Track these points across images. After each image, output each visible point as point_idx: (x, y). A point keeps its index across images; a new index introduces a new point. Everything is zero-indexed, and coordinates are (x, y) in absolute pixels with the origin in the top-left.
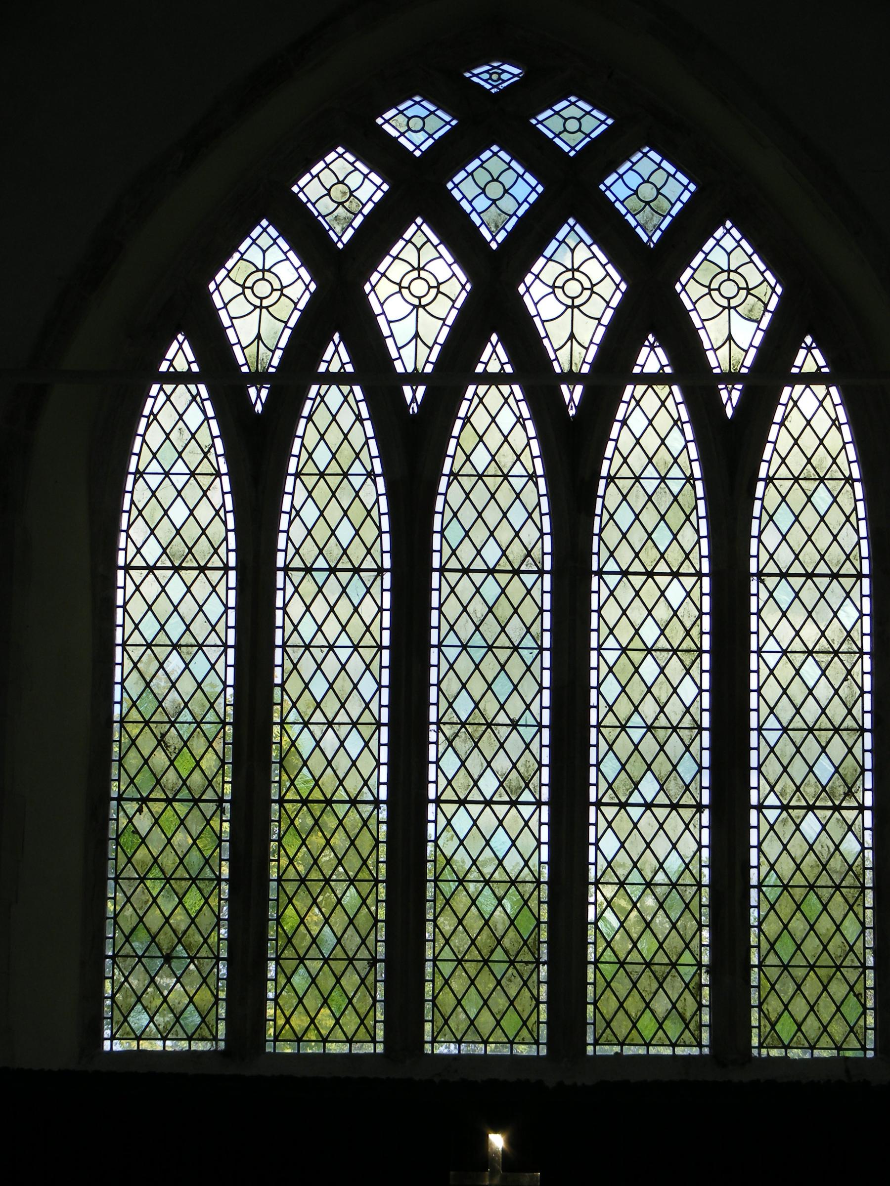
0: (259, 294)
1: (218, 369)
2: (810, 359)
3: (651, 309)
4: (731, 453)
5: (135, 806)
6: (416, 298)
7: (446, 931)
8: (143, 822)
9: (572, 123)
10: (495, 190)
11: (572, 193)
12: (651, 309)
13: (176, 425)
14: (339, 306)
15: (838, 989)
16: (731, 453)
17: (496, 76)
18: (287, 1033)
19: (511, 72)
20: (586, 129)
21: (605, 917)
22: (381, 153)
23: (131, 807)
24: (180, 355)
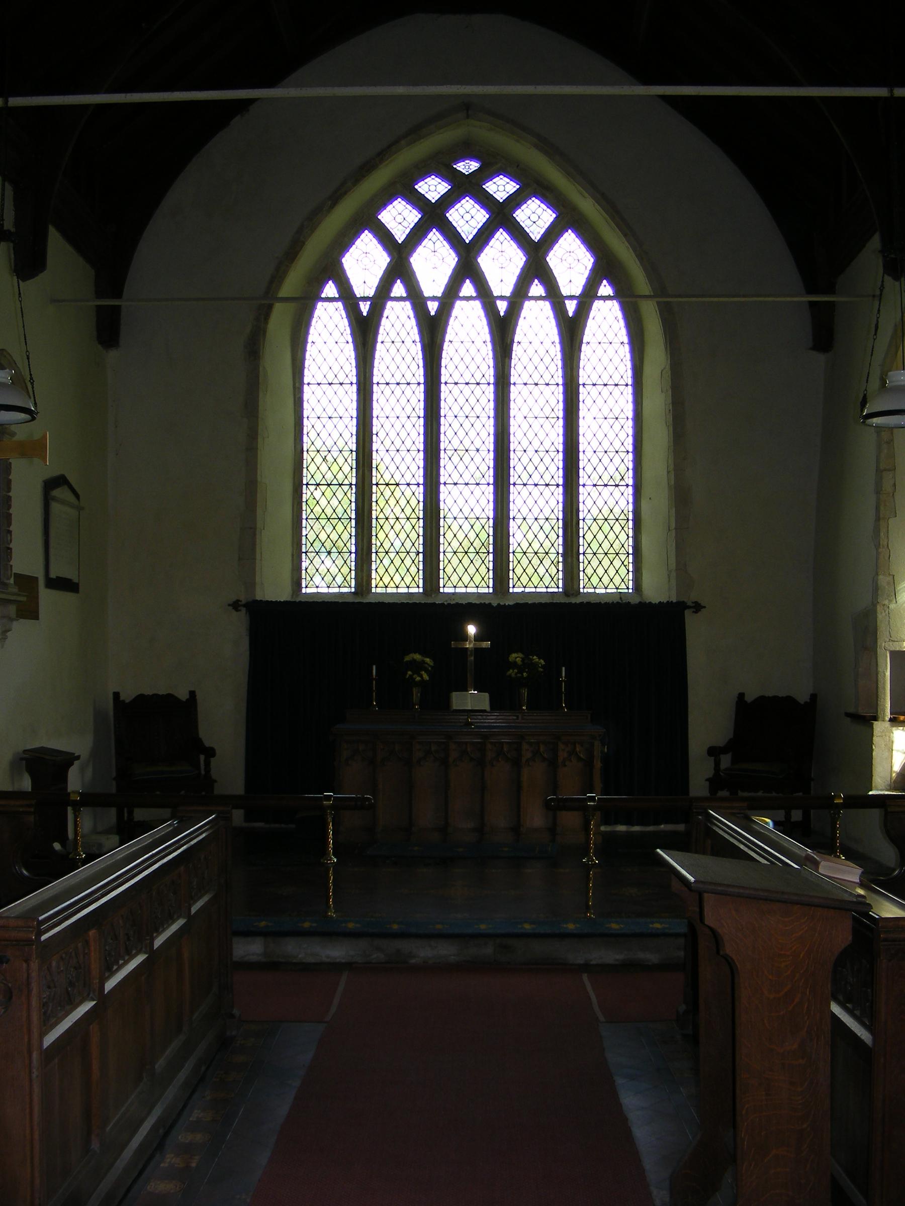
0: (364, 263)
1: (347, 297)
2: (605, 289)
3: (537, 268)
4: (571, 331)
5: (314, 487)
6: (433, 264)
7: (449, 542)
8: (318, 494)
9: (501, 187)
10: (468, 217)
11: (501, 216)
12: (537, 268)
13: (329, 325)
14: (399, 268)
15: (617, 563)
16: (571, 331)
17: (468, 167)
18: (381, 584)
19: (474, 166)
20: (507, 190)
21: (517, 537)
22: (418, 201)
23: (312, 488)
24: (330, 290)
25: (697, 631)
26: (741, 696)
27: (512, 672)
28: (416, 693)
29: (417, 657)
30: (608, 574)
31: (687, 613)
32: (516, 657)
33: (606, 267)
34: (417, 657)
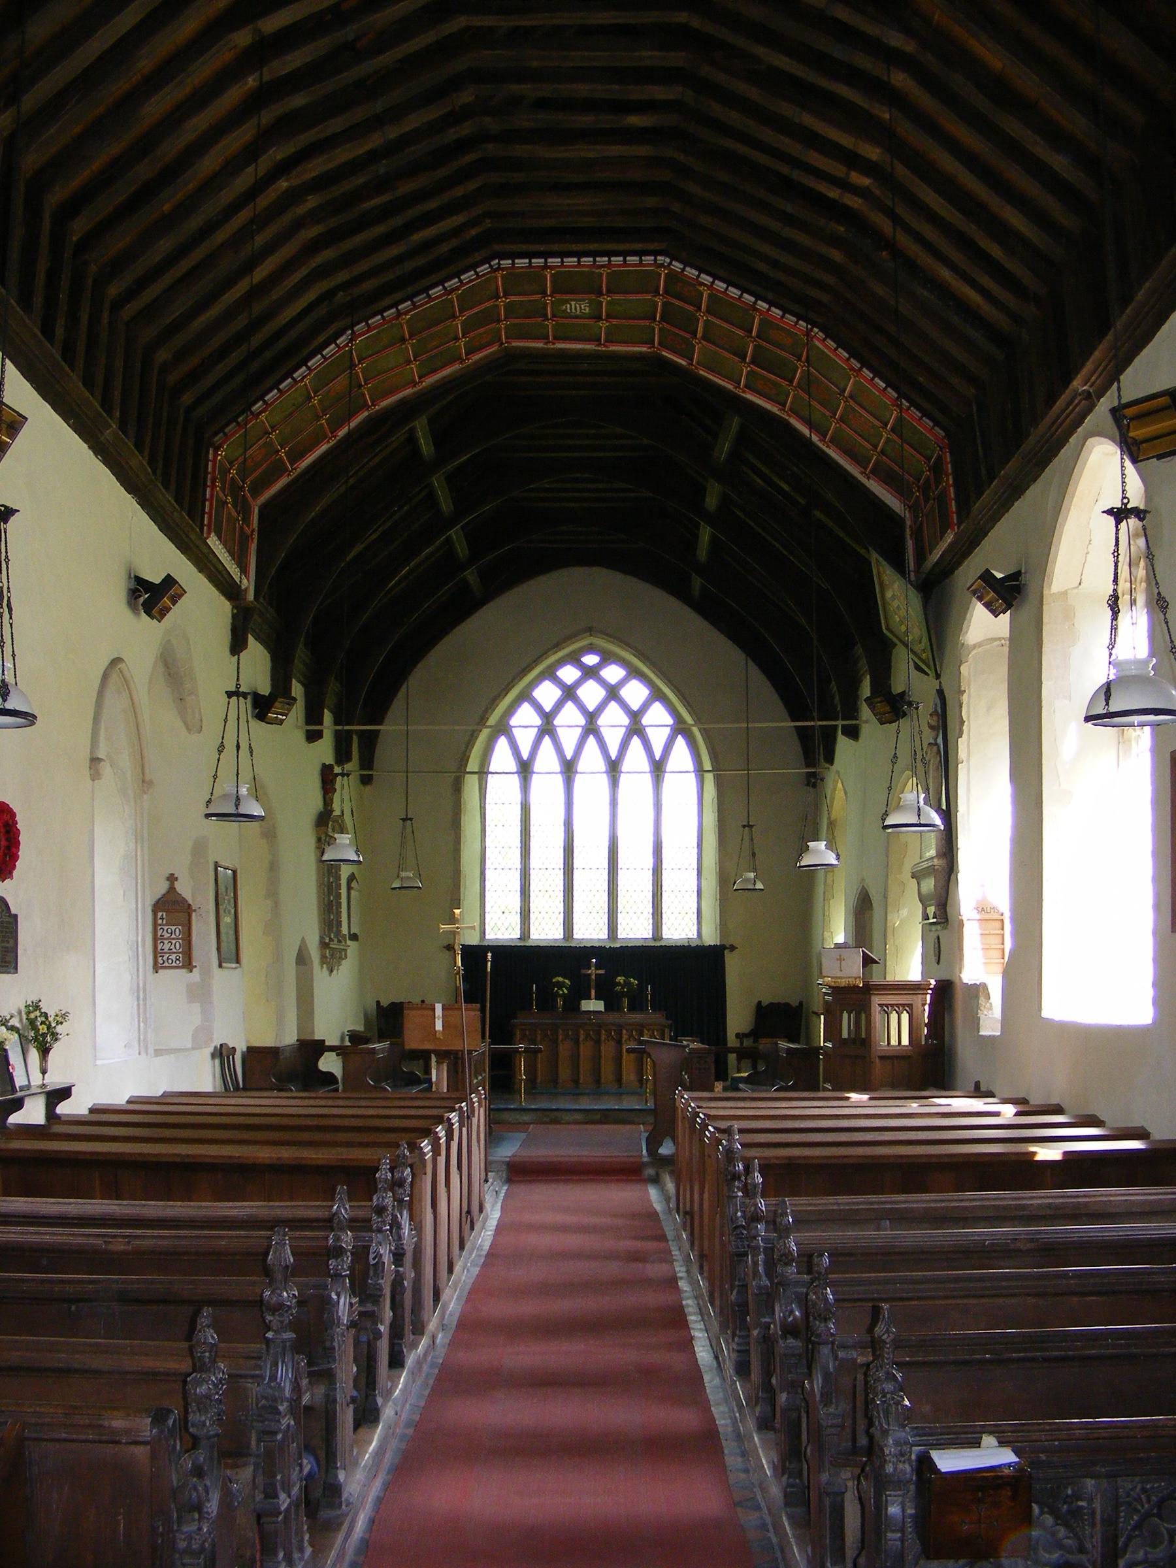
0: (525, 719)
10: (591, 694)
12: (636, 729)
16: (658, 768)
25: (732, 964)
26: (760, 1003)
27: (618, 988)
28: (560, 1002)
29: (560, 979)
30: (682, 926)
31: (726, 952)
32: (620, 979)
33: (679, 728)
34: (560, 979)
